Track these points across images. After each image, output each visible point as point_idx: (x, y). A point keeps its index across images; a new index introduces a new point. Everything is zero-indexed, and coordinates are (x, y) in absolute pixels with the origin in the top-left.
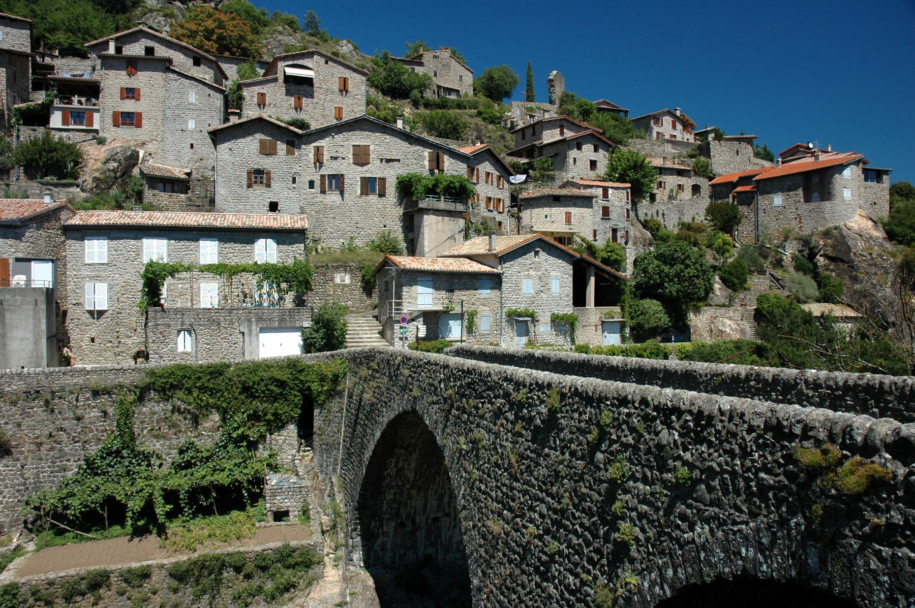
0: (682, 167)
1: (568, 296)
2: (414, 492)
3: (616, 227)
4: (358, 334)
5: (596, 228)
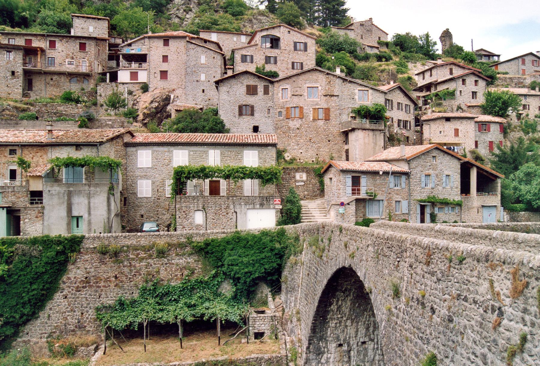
1: (457, 188)
2: (349, 323)
5: (477, 139)
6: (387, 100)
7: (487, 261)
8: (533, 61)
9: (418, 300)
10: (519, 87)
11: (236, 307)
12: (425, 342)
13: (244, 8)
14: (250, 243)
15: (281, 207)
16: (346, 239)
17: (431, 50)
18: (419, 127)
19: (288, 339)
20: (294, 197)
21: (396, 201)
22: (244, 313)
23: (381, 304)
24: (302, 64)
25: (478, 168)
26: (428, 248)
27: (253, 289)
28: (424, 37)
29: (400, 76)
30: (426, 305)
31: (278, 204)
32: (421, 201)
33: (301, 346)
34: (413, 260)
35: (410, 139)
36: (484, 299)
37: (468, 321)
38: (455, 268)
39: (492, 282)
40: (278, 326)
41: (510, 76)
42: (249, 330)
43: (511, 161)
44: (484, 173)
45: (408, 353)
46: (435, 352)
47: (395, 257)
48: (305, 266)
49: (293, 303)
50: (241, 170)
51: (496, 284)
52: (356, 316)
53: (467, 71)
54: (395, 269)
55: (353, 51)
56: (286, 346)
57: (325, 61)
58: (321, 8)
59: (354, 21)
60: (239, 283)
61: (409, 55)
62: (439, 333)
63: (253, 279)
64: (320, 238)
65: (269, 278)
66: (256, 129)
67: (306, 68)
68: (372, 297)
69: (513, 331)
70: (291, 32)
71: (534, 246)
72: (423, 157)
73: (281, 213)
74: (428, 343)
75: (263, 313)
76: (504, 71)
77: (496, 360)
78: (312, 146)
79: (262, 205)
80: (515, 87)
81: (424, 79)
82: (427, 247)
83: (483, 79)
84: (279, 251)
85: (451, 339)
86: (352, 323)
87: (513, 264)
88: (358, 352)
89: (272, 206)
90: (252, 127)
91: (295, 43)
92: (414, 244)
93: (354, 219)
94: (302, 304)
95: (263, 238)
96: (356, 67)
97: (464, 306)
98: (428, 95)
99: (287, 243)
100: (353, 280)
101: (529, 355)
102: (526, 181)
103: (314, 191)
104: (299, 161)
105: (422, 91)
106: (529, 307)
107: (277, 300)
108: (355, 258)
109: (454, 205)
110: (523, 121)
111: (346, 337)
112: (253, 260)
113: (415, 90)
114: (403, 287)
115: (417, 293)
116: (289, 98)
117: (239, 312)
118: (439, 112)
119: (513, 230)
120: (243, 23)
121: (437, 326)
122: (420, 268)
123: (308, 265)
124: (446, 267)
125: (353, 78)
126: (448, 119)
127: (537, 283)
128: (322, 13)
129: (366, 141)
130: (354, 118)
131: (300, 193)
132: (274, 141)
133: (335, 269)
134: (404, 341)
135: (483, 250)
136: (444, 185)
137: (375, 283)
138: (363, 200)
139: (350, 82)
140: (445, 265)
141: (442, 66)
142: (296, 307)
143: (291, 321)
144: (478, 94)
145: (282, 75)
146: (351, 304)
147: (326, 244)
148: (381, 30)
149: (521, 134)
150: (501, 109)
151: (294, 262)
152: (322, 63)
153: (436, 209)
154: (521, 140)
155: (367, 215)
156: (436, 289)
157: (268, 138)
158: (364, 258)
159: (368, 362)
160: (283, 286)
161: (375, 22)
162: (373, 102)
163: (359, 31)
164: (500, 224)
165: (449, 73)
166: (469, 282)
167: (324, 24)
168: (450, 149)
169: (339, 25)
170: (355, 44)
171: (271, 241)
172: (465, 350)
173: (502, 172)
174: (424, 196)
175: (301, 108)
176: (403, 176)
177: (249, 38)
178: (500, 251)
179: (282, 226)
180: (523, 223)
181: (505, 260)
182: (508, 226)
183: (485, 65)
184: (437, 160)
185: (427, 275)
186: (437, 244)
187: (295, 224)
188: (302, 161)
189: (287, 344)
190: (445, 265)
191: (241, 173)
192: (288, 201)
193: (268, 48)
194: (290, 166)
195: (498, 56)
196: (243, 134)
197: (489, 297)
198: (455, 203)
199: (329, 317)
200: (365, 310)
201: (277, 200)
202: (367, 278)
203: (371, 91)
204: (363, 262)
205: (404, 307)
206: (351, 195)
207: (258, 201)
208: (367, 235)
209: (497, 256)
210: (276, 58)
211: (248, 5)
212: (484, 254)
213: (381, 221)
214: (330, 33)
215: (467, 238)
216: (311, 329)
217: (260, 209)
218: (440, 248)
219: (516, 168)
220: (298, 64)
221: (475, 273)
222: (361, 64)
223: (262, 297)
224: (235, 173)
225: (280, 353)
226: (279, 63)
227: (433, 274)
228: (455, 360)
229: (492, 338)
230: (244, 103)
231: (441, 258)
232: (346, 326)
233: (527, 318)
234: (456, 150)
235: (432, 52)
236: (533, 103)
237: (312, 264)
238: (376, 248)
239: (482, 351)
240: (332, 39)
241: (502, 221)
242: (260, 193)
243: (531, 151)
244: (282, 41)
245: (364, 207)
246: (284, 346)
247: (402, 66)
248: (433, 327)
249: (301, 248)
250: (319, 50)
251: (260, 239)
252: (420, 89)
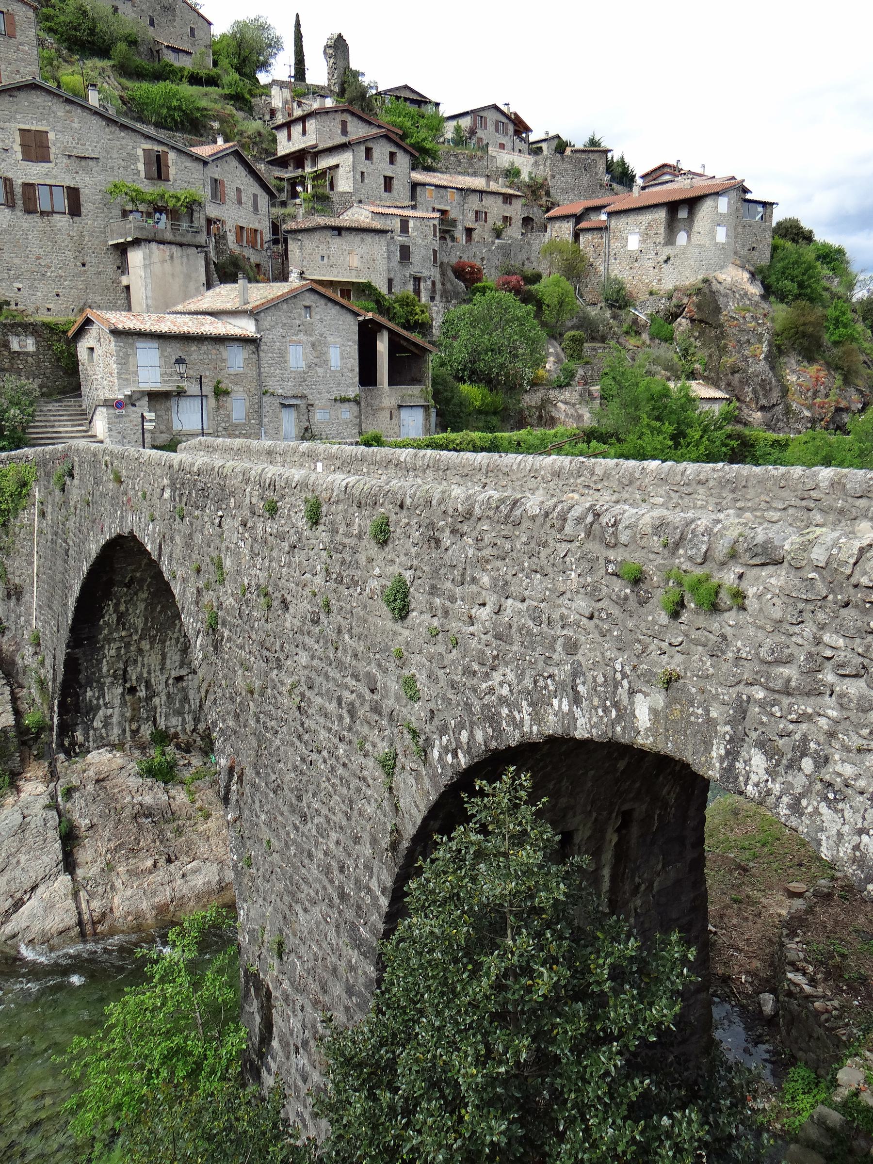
0: (511, 191)
1: (352, 370)
2: (145, 645)
3: (419, 275)
4: (53, 426)
5: (392, 276)
8: (497, 122)
53: (375, 131)
72: (285, 306)
83: (405, 151)
86: (152, 643)
142: (31, 625)
144: (395, 182)
184: (313, 313)
199: (101, 637)
218: (294, 485)
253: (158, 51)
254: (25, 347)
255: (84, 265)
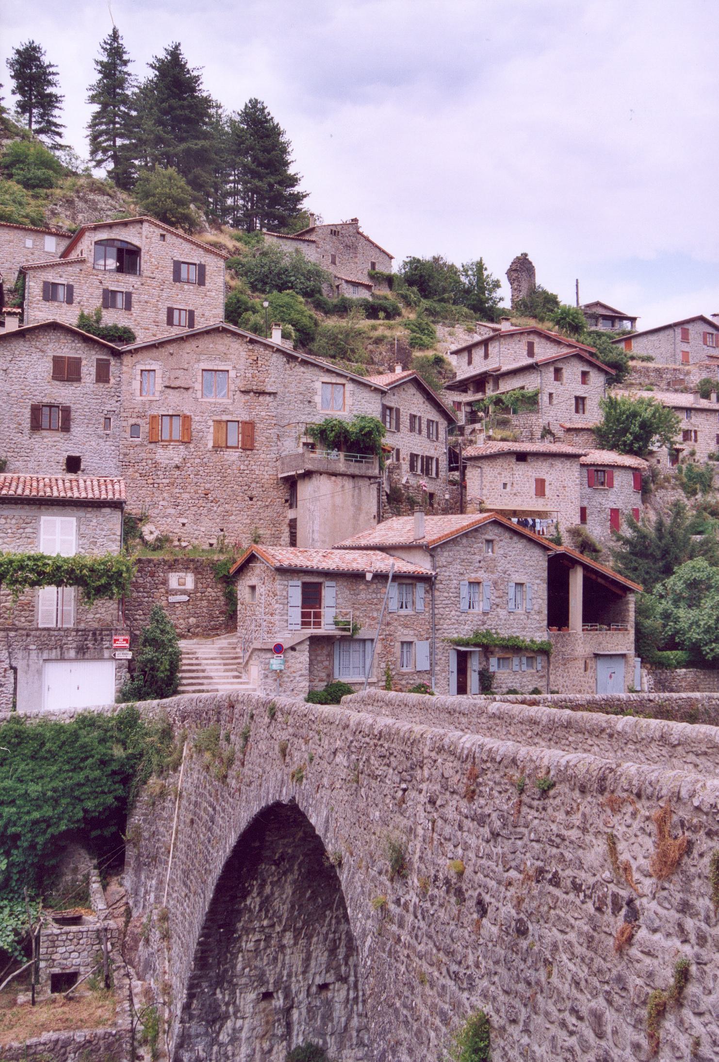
1: (539, 613)
5: (585, 504)
6: (386, 408)
7: (602, 790)
8: (705, 334)
9: (447, 882)
10: (676, 391)
11: (7, 911)
12: (465, 986)
13: (55, 171)
14: (48, 745)
15: (129, 655)
16: (284, 735)
17: (488, 299)
18: (457, 473)
19: (138, 986)
20: (163, 631)
21: (403, 643)
22: (27, 926)
23: (363, 893)
24: (191, 313)
25: (586, 568)
26: (470, 759)
27: (53, 862)
28: (472, 269)
29: (417, 354)
30: (467, 896)
31: (124, 648)
32: (458, 643)
33: (171, 1003)
34: (438, 787)
35: (436, 499)
36: (595, 879)
37: (562, 931)
38: (531, 807)
39: (612, 841)
40: (115, 955)
41: (657, 366)
42: (37, 969)
43: (658, 553)
44: (600, 580)
45: (426, 1012)
46: (488, 1009)
47: (397, 779)
48: (184, 802)
49: (152, 895)
50: (31, 563)
51: (621, 846)
52: (305, 922)
53: (565, 351)
54: (396, 808)
55: (312, 291)
56: (132, 1004)
57: (246, 310)
58: (240, 187)
59: (318, 223)
60: (17, 848)
61: (438, 307)
62: (497, 963)
63: (53, 836)
64: (223, 733)
65: (94, 833)
66: (73, 464)
67: (200, 325)
68: (343, 876)
69: (660, 955)
70: (168, 236)
71: (705, 753)
72: (464, 541)
73: (130, 670)
74: (471, 988)
75: (75, 924)
76: (644, 354)
77: (624, 1025)
78: (210, 510)
79: (82, 653)
80: (667, 390)
81: (470, 363)
82: (469, 757)
83: (600, 369)
84: (123, 765)
85: (522, 976)
86: (296, 938)
87: (659, 799)
88: (308, 1011)
89: (106, 654)
90: (63, 459)
91: (177, 265)
92: (441, 750)
93: (305, 684)
94: (174, 895)
95: (82, 732)
96: (320, 329)
97: (553, 896)
98: (478, 401)
99: (142, 745)
100: (301, 834)
101: (695, 1014)
102: (691, 599)
103: (212, 617)
104: (177, 543)
105: (465, 391)
106: (692, 900)
107: (114, 887)
108: (304, 781)
109: (533, 651)
110: (684, 466)
111: (281, 973)
112: (55, 790)
113: (450, 388)
114: (415, 852)
115: (446, 866)
116: (157, 394)
117: (12, 923)
118: (503, 440)
119: (663, 712)
120: (51, 206)
121: (490, 944)
122: (452, 809)
123: (193, 798)
124: (511, 803)
125: (310, 352)
126: (522, 457)
127: (711, 844)
128: (243, 199)
129: (338, 500)
130: (311, 447)
131: (178, 620)
132: (117, 496)
133: (256, 809)
134: (416, 983)
135: (593, 766)
136: (511, 605)
137: (350, 842)
138: (328, 640)
139: (305, 363)
140: (509, 799)
141: (511, 335)
142: (161, 903)
143: (147, 941)
144: (588, 402)
145: (142, 338)
146: (293, 893)
147: (237, 747)
148: (377, 247)
149: (679, 495)
150: (637, 438)
151: (158, 790)
152: (240, 315)
153: (493, 661)
154: (678, 509)
155: (336, 675)
156: (489, 857)
157: (103, 487)
158: (325, 781)
159: (332, 1034)
160: (130, 853)
161: (365, 228)
162: (355, 413)
163: (329, 246)
164: (633, 696)
165: (525, 353)
166: (564, 840)
167: (245, 223)
168: (524, 524)
169: (282, 230)
170: (316, 274)
171: (102, 741)
172: (555, 1003)
173: (638, 577)
174: (465, 632)
175: (187, 419)
176: (418, 584)
177: (65, 243)
178: (630, 768)
179: (130, 704)
180: (683, 695)
181: (640, 790)
182: (651, 701)
183: (604, 338)
184: (496, 548)
185: (467, 823)
186: (491, 749)
187: (162, 696)
188: (184, 544)
189: (136, 1000)
190: (509, 799)
191: (32, 570)
192: (147, 642)
193: (110, 271)
194: (157, 556)
195: (633, 320)
196: (40, 476)
197: (607, 875)
198: (535, 647)
199: (240, 925)
200: (328, 906)
201: (121, 638)
202: (331, 829)
203: (350, 386)
204: (323, 792)
205: (415, 899)
206: (299, 627)
207: (71, 642)
208: (333, 726)
209: (623, 779)
210: (128, 296)
211: (64, 164)
212: (595, 774)
213: (368, 690)
214: (260, 246)
215: (560, 733)
216: (195, 959)
217: (76, 659)
218: (498, 759)
219: (668, 571)
220: (183, 313)
221: (576, 819)
222: (331, 323)
223: (74, 881)
224: (16, 571)
225: (115, 1024)
226: (135, 307)
227: (481, 820)
228: (532, 1028)
229: (615, 972)
230: (46, 400)
231: (500, 784)
232: (282, 947)
233: (690, 924)
234: (538, 528)
235: (490, 303)
236: (704, 426)
237: (201, 795)
238: (353, 757)
239: (593, 1004)
240: (265, 260)
241: (638, 688)
242: (78, 621)
243: (700, 533)
244: (144, 257)
245: (330, 656)
246: (126, 1005)
247: (422, 331)
248: (482, 948)
249: (175, 756)
250: (233, 283)
251: (76, 735)
252: (462, 386)
253: (338, 287)
254: (184, 584)
255: (251, 499)
